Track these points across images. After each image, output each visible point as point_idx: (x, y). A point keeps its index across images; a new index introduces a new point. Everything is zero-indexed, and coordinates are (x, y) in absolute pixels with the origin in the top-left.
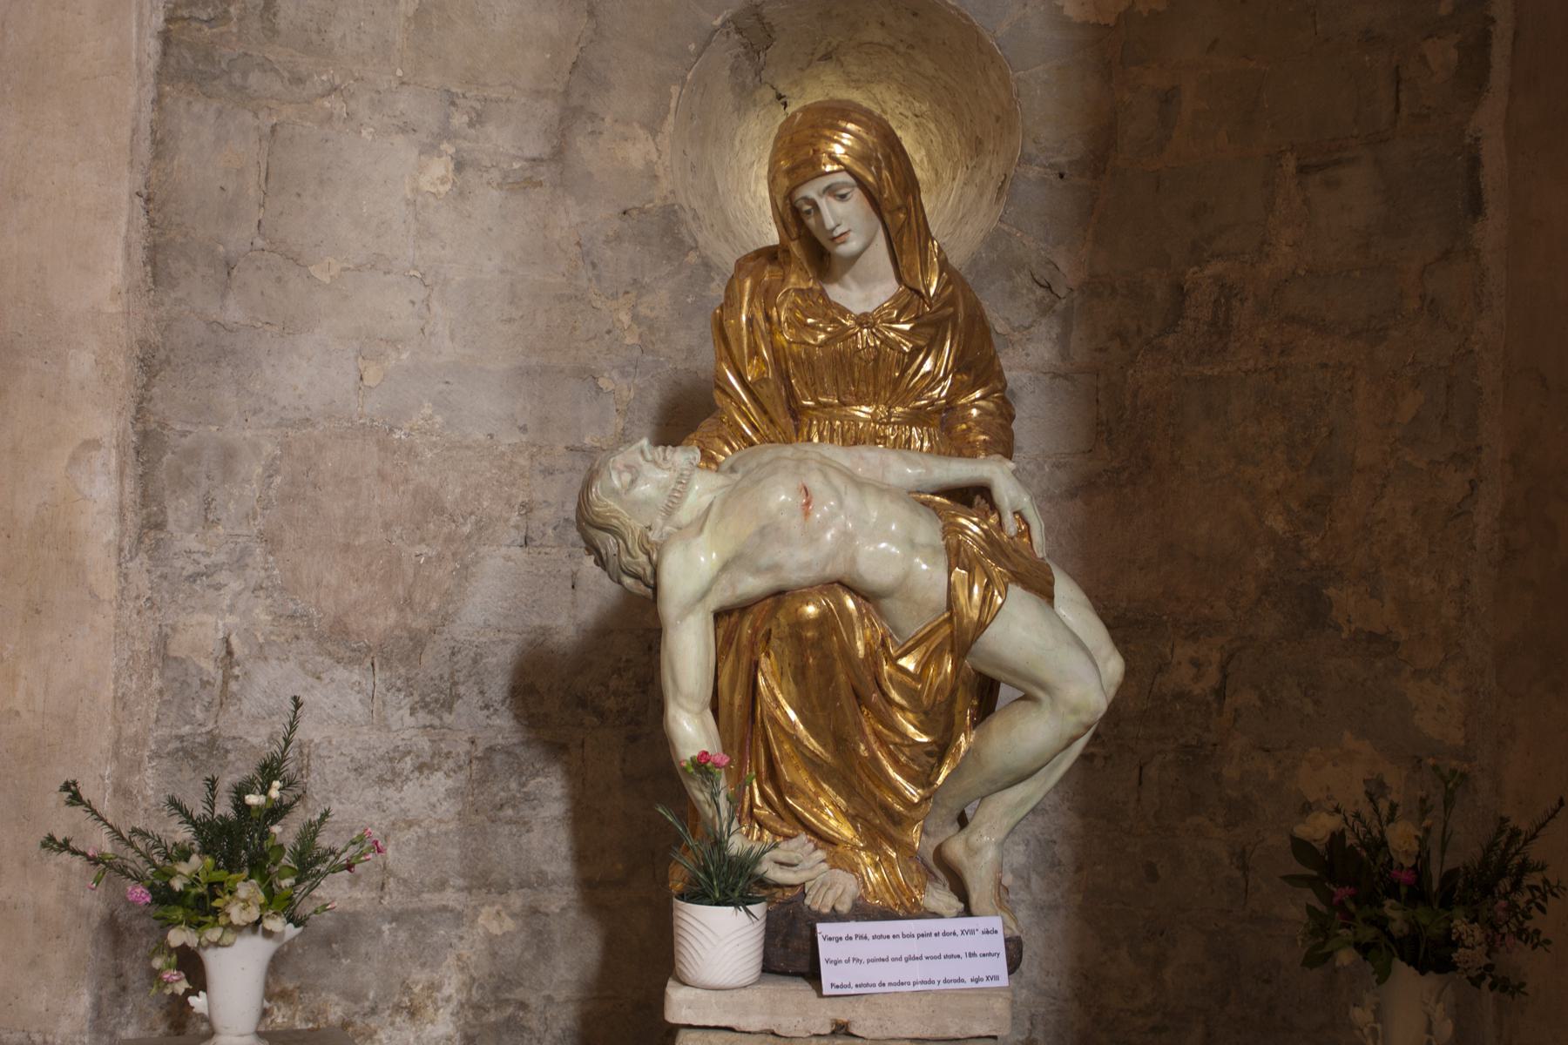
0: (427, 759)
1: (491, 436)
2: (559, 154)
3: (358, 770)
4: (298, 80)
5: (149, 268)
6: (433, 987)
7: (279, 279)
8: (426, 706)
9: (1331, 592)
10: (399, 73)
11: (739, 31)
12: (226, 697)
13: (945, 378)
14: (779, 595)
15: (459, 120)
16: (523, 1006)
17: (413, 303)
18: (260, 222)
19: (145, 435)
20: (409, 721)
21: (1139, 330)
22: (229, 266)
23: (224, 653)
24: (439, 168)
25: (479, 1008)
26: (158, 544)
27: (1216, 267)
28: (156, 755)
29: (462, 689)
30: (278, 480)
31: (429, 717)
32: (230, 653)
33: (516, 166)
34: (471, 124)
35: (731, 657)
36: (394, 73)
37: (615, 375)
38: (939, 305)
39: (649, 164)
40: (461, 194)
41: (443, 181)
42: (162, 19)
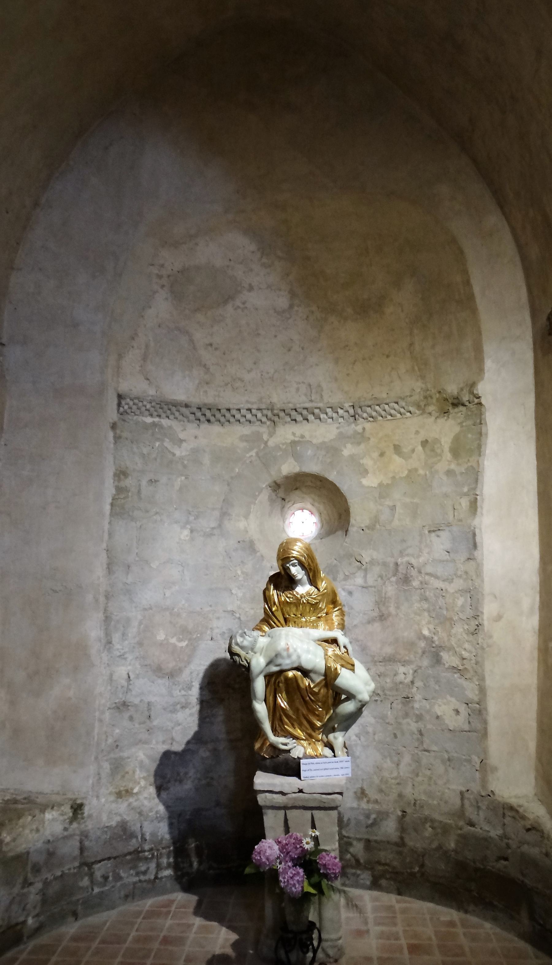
0: (184, 705)
1: (201, 609)
2: (220, 526)
3: (165, 709)
4: (147, 511)
5: (108, 570)
6: (186, 773)
7: (142, 569)
8: (183, 689)
9: (442, 654)
10: (175, 507)
11: (270, 487)
12: (128, 690)
13: (325, 608)
14: (282, 672)
15: (192, 518)
16: (212, 778)
17: (179, 571)
18: (137, 553)
19: (106, 617)
20: (179, 693)
21: (386, 575)
22: (129, 567)
23: (128, 677)
24: (186, 532)
25: (199, 779)
26: (110, 648)
27: (406, 559)
28: (109, 708)
29: (194, 684)
30: (142, 626)
31: (185, 692)
32: (129, 677)
33: (207, 530)
34: (195, 519)
35: (269, 687)
36: (174, 507)
37: (237, 589)
38: (323, 590)
39: (245, 528)
40: (192, 539)
41: (187, 536)
42: (111, 499)
